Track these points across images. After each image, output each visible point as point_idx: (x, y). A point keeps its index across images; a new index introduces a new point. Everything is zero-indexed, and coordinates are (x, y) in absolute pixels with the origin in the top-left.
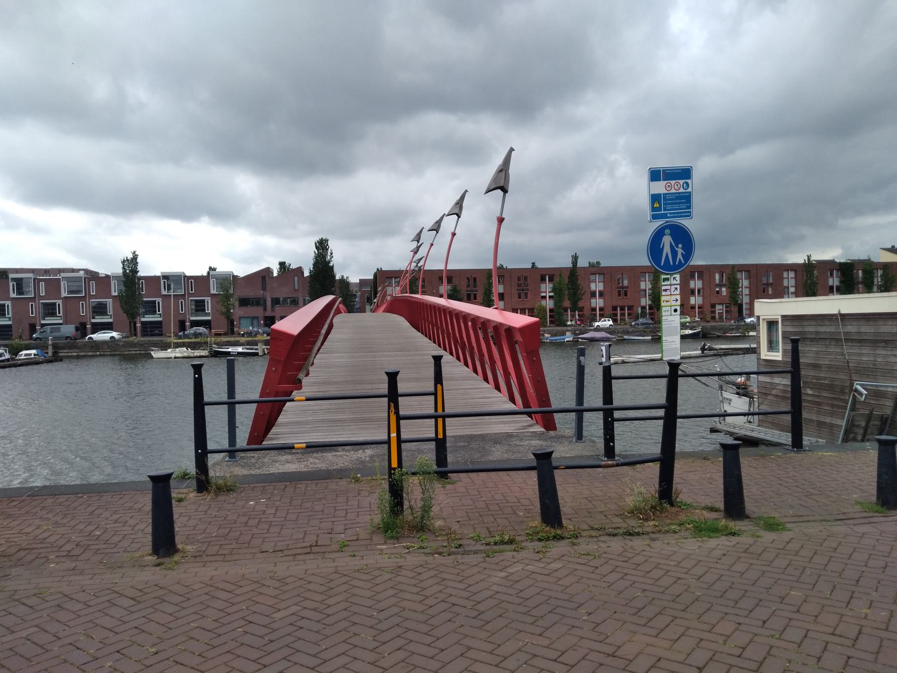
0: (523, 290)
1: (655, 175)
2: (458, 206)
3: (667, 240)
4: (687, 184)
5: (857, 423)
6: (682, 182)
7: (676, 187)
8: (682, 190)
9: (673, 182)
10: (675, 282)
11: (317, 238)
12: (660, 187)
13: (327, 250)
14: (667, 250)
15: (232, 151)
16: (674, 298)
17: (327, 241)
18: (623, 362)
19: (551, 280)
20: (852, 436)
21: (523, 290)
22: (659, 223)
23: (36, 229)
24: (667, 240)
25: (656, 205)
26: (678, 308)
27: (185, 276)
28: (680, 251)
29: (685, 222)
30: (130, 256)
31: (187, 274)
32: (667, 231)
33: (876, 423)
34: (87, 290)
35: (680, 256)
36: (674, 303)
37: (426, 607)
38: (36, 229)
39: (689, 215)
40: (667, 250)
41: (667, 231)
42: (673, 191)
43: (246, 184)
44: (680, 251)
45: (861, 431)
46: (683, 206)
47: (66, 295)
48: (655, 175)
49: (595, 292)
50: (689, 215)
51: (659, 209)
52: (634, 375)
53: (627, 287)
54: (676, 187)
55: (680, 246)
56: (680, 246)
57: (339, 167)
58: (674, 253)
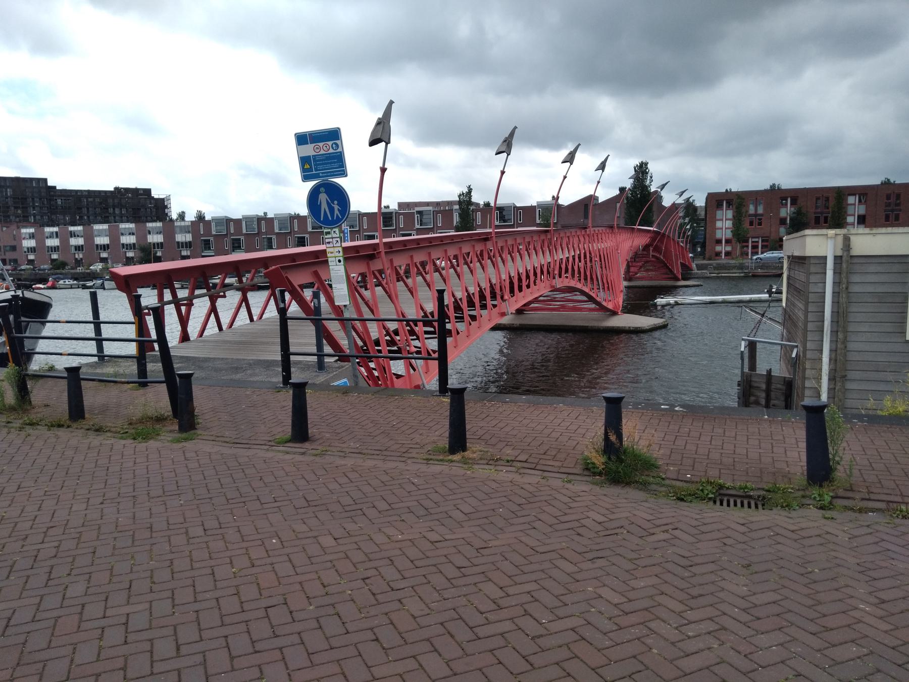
0: (892, 211)
1: (302, 139)
2: (505, 144)
3: (323, 197)
4: (337, 145)
5: (756, 385)
6: (330, 143)
7: (325, 148)
8: (331, 151)
9: (321, 144)
10: (334, 235)
11: (637, 162)
12: (309, 150)
13: (647, 173)
14: (324, 206)
15: (594, 73)
16: (336, 249)
17: (646, 164)
18: (677, 304)
19: (793, 203)
20: (752, 399)
21: (892, 211)
22: (311, 184)
23: (428, 166)
24: (323, 197)
25: (307, 166)
26: (342, 259)
27: (515, 207)
28: (336, 207)
29: (339, 181)
30: (465, 190)
31: (518, 205)
32: (322, 189)
33: (779, 386)
34: (435, 222)
35: (336, 212)
36: (337, 254)
37: (609, 558)
38: (428, 166)
39: (344, 174)
40: (324, 206)
41: (322, 189)
42: (322, 152)
43: (606, 106)
44: (336, 207)
45: (763, 395)
46: (336, 165)
47: (419, 227)
48: (302, 139)
49: (785, 219)
50: (344, 174)
51: (310, 170)
52: (111, 325)
53: (762, 215)
54: (325, 148)
55: (336, 202)
56: (336, 202)
57: (702, 77)
58: (332, 210)
